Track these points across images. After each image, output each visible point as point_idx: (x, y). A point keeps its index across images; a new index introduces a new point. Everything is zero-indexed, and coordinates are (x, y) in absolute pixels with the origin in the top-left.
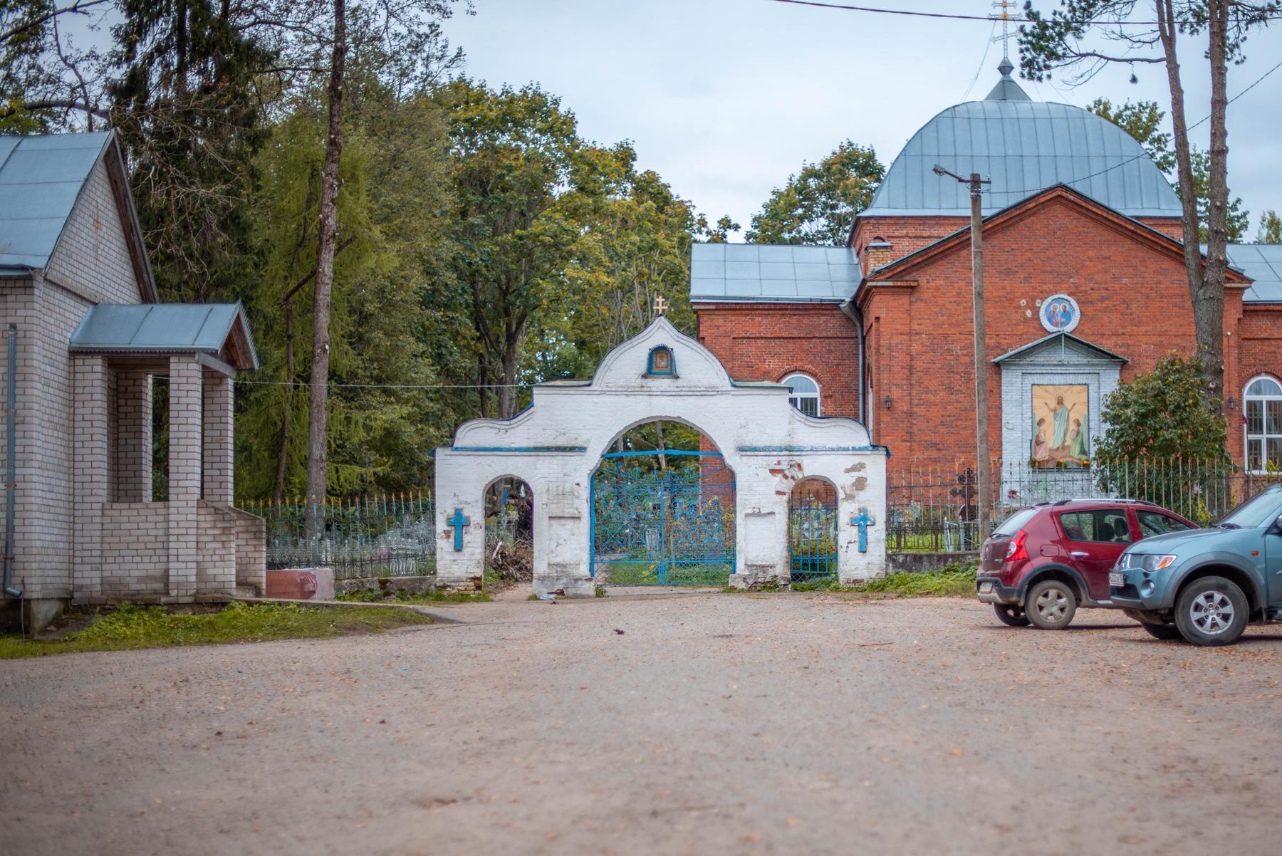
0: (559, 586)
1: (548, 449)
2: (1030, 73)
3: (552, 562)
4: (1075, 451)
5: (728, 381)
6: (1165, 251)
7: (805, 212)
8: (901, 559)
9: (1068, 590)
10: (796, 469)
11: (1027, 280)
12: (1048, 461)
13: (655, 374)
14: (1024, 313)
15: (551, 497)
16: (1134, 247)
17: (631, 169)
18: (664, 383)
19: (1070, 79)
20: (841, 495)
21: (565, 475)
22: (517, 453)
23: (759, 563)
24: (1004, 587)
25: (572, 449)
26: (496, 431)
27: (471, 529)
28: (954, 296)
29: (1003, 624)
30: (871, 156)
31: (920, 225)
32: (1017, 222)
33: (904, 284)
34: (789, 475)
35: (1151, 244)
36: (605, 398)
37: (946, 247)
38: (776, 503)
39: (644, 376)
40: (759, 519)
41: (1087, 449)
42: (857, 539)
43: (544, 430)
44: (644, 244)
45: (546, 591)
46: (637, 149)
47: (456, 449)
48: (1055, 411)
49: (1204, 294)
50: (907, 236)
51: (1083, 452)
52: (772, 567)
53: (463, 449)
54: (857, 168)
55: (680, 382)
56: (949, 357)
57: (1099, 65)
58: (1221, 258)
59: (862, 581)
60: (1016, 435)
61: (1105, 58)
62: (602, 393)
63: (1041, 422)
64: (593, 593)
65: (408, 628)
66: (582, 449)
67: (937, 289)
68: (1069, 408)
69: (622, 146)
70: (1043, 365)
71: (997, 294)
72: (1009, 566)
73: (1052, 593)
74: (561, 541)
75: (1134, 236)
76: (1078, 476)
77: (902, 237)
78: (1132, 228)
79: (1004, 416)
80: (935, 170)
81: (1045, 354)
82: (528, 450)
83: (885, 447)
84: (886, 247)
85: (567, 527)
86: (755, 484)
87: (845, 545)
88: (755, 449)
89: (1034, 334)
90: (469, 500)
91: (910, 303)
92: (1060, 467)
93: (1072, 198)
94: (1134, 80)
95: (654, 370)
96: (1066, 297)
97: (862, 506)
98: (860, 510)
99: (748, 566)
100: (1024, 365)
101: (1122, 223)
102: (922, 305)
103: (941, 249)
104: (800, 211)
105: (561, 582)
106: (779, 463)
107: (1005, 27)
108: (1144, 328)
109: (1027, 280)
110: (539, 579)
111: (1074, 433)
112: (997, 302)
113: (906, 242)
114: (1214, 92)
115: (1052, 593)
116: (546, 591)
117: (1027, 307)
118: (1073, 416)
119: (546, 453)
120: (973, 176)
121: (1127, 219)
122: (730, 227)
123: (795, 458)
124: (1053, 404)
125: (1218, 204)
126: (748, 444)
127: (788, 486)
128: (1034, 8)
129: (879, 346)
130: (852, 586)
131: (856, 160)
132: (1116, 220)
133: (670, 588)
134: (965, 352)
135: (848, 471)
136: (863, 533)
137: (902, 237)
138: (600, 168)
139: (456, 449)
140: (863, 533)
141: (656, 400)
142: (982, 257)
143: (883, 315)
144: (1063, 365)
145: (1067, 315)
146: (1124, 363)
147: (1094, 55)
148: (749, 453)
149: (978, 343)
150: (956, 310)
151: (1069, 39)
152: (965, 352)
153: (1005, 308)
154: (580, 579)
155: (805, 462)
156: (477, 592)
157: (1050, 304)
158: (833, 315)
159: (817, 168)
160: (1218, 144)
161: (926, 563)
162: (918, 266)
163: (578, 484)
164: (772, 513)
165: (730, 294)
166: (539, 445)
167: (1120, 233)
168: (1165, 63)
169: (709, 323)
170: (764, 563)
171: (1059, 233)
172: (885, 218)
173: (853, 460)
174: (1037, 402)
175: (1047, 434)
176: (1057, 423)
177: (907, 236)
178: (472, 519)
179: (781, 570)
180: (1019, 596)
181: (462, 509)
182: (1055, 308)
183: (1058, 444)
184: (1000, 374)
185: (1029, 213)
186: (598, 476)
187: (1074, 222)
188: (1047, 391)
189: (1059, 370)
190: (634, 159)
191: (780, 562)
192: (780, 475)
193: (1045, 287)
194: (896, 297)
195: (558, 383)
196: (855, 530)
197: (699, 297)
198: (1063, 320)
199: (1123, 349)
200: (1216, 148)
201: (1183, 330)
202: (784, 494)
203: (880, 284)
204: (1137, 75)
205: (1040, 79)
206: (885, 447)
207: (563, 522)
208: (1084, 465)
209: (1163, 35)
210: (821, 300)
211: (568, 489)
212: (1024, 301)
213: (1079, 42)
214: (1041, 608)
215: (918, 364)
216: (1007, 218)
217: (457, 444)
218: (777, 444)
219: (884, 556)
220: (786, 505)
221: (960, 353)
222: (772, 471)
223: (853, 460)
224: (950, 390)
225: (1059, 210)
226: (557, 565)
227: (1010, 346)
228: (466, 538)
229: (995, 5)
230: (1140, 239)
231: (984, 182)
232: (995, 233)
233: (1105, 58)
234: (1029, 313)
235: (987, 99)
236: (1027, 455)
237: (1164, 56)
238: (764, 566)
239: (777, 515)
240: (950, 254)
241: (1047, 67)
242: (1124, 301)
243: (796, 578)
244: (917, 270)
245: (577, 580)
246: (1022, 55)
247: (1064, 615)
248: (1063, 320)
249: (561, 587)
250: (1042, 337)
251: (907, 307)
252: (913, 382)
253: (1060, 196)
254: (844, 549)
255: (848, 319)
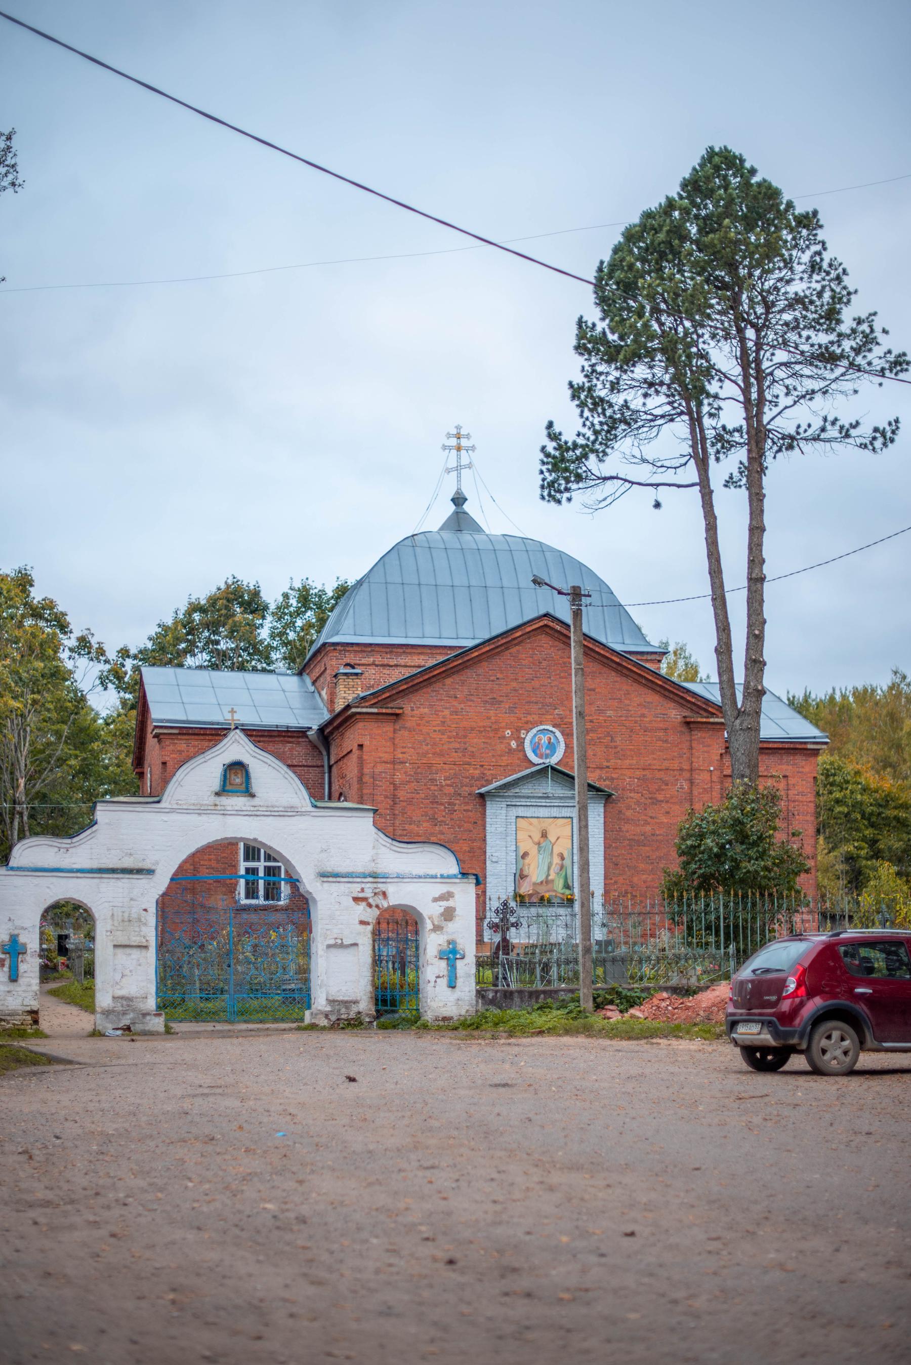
0: (125, 1021)
1: (113, 871)
2: (550, 495)
3: (116, 995)
4: (559, 885)
5: (308, 801)
6: (650, 685)
7: (187, 646)
8: (491, 995)
9: (851, 1031)
10: (381, 897)
11: (511, 710)
12: (530, 896)
13: (228, 791)
14: (509, 745)
15: (116, 924)
16: (618, 679)
17: (28, 596)
18: (238, 802)
19: (592, 503)
20: (429, 925)
21: (132, 899)
22: (79, 875)
23: (341, 998)
24: (782, 1028)
25: (139, 871)
26: (56, 849)
27: (28, 957)
28: (438, 725)
29: (750, 1069)
30: (256, 594)
31: (386, 653)
32: (502, 651)
33: (389, 711)
34: (373, 904)
35: (636, 677)
36: (174, 817)
37: (431, 674)
38: (359, 934)
39: (217, 794)
40: (340, 951)
41: (571, 884)
42: (446, 973)
43: (109, 850)
44: (46, 671)
45: (110, 1026)
46: (35, 575)
47: (12, 869)
48: (539, 844)
49: (741, 724)
50: (374, 664)
51: (567, 886)
52: (356, 1002)
53: (19, 869)
54: (241, 604)
55: (256, 801)
56: (432, 788)
57: (623, 489)
58: (760, 688)
59: (450, 1018)
60: (501, 867)
61: (630, 482)
62: (172, 811)
63: (525, 855)
64: (162, 1029)
65: (28, 1070)
66: (150, 872)
67: (421, 717)
68: (553, 841)
69: (20, 572)
70: (528, 797)
71: (481, 724)
72: (785, 1006)
73: (836, 1035)
74: (127, 972)
75: (619, 668)
76: (561, 911)
77: (369, 665)
78: (618, 660)
79: (488, 848)
80: (535, 581)
81: (530, 786)
82: (91, 871)
83: (474, 875)
84: (356, 674)
85: (133, 956)
86: (338, 913)
87: (433, 979)
88: (337, 875)
89: (519, 766)
90: (25, 925)
91: (395, 731)
92: (543, 902)
93: (558, 628)
94: (657, 505)
95: (228, 788)
96: (551, 728)
97: (450, 937)
98: (449, 943)
99: (331, 1002)
100: (509, 796)
101: (607, 655)
102: (406, 733)
103: (427, 677)
104: (183, 645)
105: (128, 1017)
106: (363, 890)
107: (459, 458)
108: (627, 762)
109: (511, 710)
110: (103, 1013)
111: (558, 867)
112: (481, 732)
113: (372, 670)
114: (751, 519)
115: (836, 1035)
116: (110, 1026)
117: (512, 737)
118: (556, 850)
119: (111, 876)
120: (574, 588)
121: (617, 653)
122: (128, 656)
123: (380, 885)
124: (537, 837)
125: (757, 632)
126: (329, 869)
127: (371, 915)
128: (557, 428)
129: (362, 775)
130: (441, 1023)
131: (242, 597)
132: (602, 652)
133: (212, 1024)
134: (448, 782)
135: (436, 900)
136: (452, 967)
137: (369, 665)
138: (5, 592)
139: (12, 869)
140: (452, 967)
141: (230, 820)
142: (583, 675)
143: (366, 743)
144: (548, 797)
145: (552, 747)
146: (608, 797)
147: (617, 478)
148: (331, 879)
149: (579, 766)
150: (441, 740)
151: (592, 462)
152: (448, 782)
153: (490, 738)
154: (148, 1014)
155: (391, 889)
156: (34, 1027)
157: (535, 735)
158: (298, 743)
159: (203, 602)
160: (756, 571)
161: (517, 999)
162: (402, 693)
163: (145, 910)
164: (356, 945)
165: (191, 718)
166: (103, 866)
167: (604, 664)
168: (698, 488)
169: (171, 748)
170: (346, 999)
171: (544, 663)
172: (352, 644)
173: (440, 889)
174: (521, 835)
175: (532, 867)
176: (541, 857)
177: (374, 664)
178: (29, 946)
179: (365, 1006)
180: (801, 1037)
181: (17, 935)
182: (541, 740)
183: (542, 877)
184: (484, 806)
185: (516, 641)
186: (164, 904)
187: (560, 652)
188: (531, 824)
189: (543, 802)
190: (32, 585)
191: (364, 997)
192: (364, 904)
193: (530, 718)
194: (380, 724)
195: (122, 799)
196: (443, 964)
197: (162, 721)
198: (548, 752)
199: (607, 782)
200: (754, 576)
201: (666, 764)
202: (368, 923)
203: (364, 710)
204: (660, 500)
205: (559, 502)
206: (474, 875)
207: (128, 950)
208: (568, 900)
209: (695, 455)
210: (288, 727)
211: (134, 916)
212: (509, 731)
213: (601, 465)
214: (824, 1052)
215: (402, 794)
216: (493, 646)
217: (13, 863)
218: (360, 869)
219: (474, 992)
220: (370, 935)
221: (444, 783)
222: (356, 899)
223: (440, 889)
224: (434, 820)
225: (544, 640)
226: (122, 998)
227: (495, 777)
228: (23, 967)
229: (449, 436)
230: (625, 671)
231: (585, 596)
232: (480, 661)
233: (630, 482)
234: (514, 744)
235: (441, 529)
236: (511, 889)
237: (698, 481)
238: (346, 1002)
239: (361, 947)
240: (435, 682)
241: (567, 490)
242: (608, 734)
243: (379, 1014)
244: (402, 697)
245: (145, 1015)
246: (542, 476)
247: (848, 1059)
248: (548, 752)
249: (128, 1022)
250: (527, 768)
251: (391, 735)
252: (397, 812)
253: (546, 626)
254: (432, 984)
255: (315, 747)
